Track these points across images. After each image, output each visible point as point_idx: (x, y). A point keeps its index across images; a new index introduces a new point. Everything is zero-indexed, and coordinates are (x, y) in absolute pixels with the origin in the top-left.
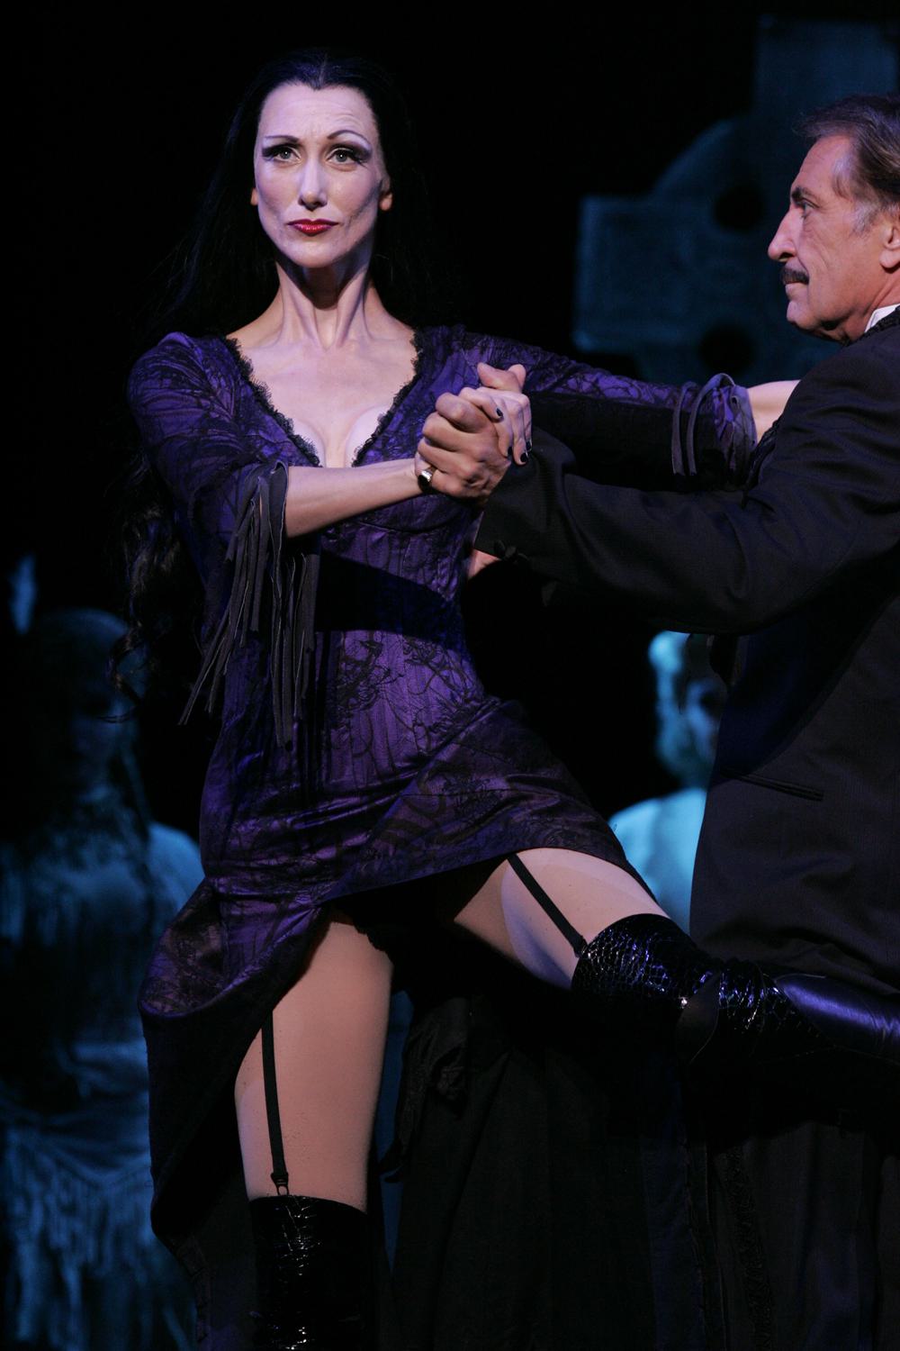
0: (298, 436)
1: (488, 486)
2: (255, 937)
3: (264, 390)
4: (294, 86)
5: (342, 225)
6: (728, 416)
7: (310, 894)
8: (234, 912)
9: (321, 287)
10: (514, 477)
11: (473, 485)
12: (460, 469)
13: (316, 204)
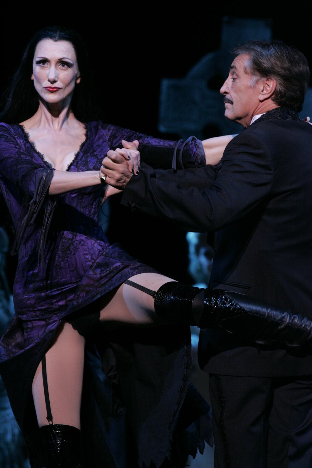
0: (46, 161)
1: (125, 182)
2: (38, 334)
3: (33, 144)
4: (47, 40)
5: (63, 89)
6: (195, 150)
7: (57, 316)
8: (29, 326)
9: (54, 109)
10: (134, 179)
11: (120, 181)
12: (115, 176)
13: (54, 82)
